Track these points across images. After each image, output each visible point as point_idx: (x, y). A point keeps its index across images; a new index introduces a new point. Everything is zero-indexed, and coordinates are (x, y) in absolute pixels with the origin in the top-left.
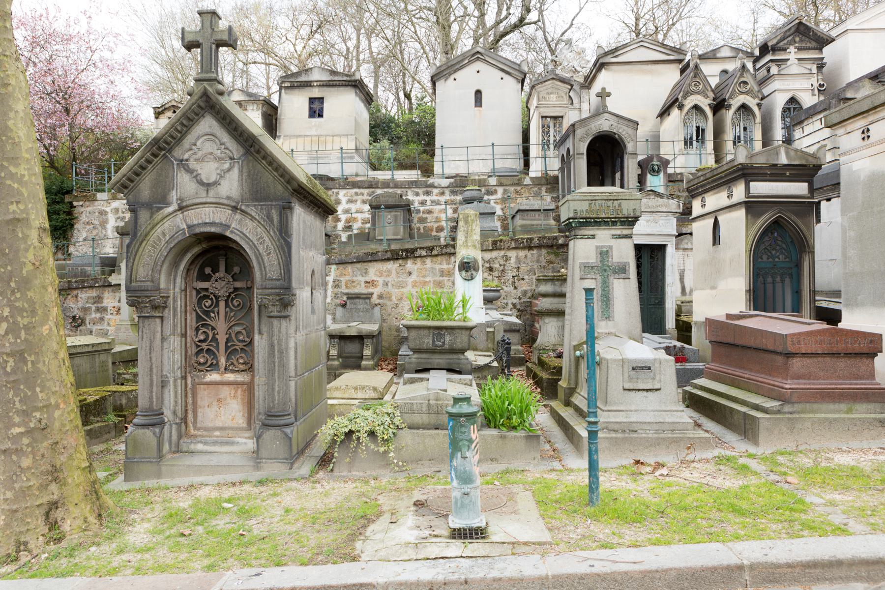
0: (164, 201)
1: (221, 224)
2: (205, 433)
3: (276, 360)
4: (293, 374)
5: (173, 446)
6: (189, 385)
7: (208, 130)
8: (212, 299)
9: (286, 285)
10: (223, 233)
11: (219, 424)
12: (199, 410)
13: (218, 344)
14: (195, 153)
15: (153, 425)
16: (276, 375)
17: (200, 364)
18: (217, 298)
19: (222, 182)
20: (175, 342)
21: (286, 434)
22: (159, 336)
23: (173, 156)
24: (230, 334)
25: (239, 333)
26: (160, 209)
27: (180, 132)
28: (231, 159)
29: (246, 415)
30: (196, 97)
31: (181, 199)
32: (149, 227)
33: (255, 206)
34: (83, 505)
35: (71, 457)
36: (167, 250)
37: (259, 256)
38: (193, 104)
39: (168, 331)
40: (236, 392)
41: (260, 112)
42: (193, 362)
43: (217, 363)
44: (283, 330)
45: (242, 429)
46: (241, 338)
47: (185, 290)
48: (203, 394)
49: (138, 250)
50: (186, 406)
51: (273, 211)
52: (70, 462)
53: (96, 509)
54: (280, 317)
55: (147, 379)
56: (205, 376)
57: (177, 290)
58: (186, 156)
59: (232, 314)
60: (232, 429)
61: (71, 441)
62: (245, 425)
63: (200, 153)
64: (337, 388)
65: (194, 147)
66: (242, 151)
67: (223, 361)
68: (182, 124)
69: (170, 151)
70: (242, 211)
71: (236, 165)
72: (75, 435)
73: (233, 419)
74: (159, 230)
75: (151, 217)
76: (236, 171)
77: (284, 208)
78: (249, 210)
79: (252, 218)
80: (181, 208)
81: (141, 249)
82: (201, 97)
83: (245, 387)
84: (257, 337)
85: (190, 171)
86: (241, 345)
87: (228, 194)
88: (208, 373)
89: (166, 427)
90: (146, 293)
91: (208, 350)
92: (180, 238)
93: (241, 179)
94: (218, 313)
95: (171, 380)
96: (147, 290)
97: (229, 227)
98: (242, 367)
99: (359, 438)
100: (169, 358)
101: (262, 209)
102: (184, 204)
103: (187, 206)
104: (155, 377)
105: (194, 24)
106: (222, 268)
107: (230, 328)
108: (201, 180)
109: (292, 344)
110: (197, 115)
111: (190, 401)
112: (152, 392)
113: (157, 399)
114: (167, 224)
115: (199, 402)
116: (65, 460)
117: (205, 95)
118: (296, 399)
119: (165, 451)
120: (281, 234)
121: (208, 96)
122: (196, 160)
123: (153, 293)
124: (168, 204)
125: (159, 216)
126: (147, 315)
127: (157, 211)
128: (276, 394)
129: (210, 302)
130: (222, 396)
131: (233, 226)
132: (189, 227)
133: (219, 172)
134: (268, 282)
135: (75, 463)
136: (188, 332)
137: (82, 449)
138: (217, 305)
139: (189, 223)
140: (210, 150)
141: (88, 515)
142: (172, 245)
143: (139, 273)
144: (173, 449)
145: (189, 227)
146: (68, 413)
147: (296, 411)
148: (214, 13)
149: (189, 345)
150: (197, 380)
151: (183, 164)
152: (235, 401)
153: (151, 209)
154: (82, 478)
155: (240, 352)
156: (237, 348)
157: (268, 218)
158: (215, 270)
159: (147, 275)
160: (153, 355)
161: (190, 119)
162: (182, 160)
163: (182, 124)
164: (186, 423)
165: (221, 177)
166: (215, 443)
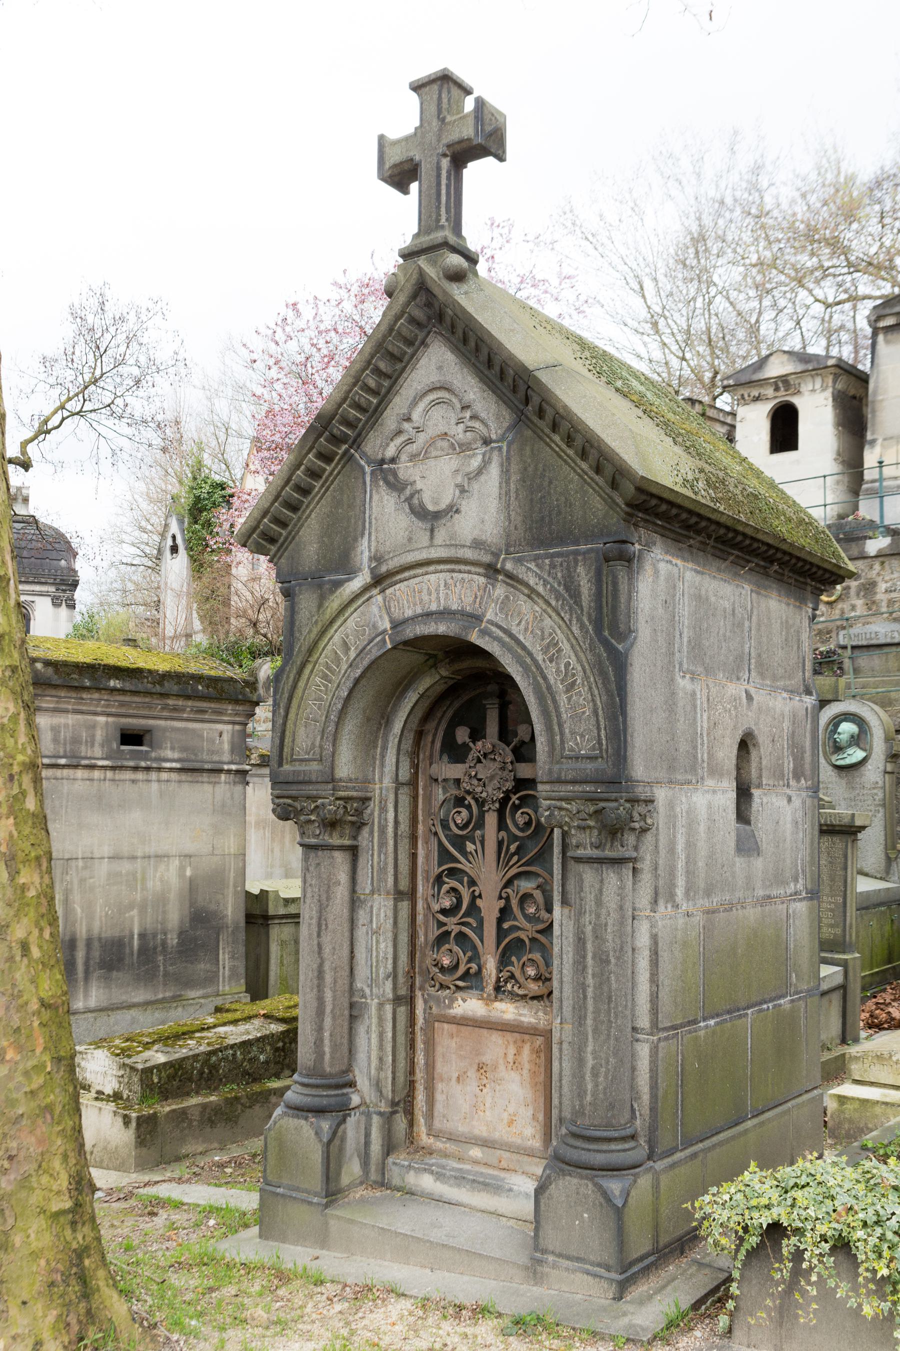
0: (344, 565)
1: (463, 613)
2: (450, 1147)
3: (590, 981)
4: (644, 1022)
5: (373, 1168)
6: (420, 1021)
7: (434, 378)
8: (469, 808)
9: (610, 771)
10: (463, 636)
11: (481, 1130)
12: (439, 1086)
13: (481, 922)
14: (410, 441)
15: (319, 1111)
17: (442, 969)
18: (481, 803)
19: (464, 506)
20: (380, 910)
21: (606, 1196)
22: (341, 893)
23: (364, 455)
24: (508, 899)
25: (525, 898)
26: (338, 584)
27: (374, 392)
28: (486, 442)
29: (541, 1117)
30: (402, 298)
31: (378, 558)
32: (315, 631)
33: (536, 559)
34: (38, 1308)
35: (24, 1183)
36: (350, 684)
37: (545, 694)
38: (397, 318)
40: (518, 1053)
41: (828, 393)
42: (429, 961)
43: (479, 971)
44: (610, 899)
45: (530, 1153)
46: (532, 910)
47: (413, 783)
48: (448, 1043)
50: (412, 1072)
51: (580, 569)
52: (23, 1194)
53: (72, 1319)
54: (600, 861)
56: (452, 1000)
58: (390, 452)
59: (513, 848)
61: (30, 1142)
63: (422, 438)
64: (880, 1057)
65: (406, 426)
66: (507, 417)
68: (377, 371)
69: (357, 442)
70: (510, 576)
71: (495, 454)
72: (43, 1128)
73: (511, 1123)
74: (336, 638)
75: (320, 606)
76: (494, 471)
77: (607, 560)
78: (520, 572)
79: (532, 594)
80: (380, 581)
81: (301, 684)
82: (414, 296)
85: (396, 485)
87: (476, 533)
88: (459, 995)
89: (351, 1121)
90: (311, 790)
92: (376, 653)
93: (505, 495)
95: (374, 1004)
96: (310, 782)
99: (798, 1255)
101: (553, 566)
102: (384, 569)
104: (328, 995)
105: (403, 117)
106: (492, 728)
107: (509, 883)
108: (422, 505)
109: (643, 940)
110: (410, 343)
111: (420, 1059)
113: (335, 1047)
114: (352, 621)
115: (440, 1067)
116: (9, 1188)
117: (422, 289)
118: (654, 1097)
119: (345, 1180)
120: (598, 629)
121: (428, 291)
122: (413, 457)
124: (352, 572)
125: (334, 603)
127: (332, 592)
128: (588, 1077)
129: (465, 813)
130: (487, 1058)
131: (489, 616)
133: (459, 479)
134: (567, 765)
135: (35, 1198)
136: (420, 888)
137: (57, 1164)
138: (480, 824)
139: (397, 614)
140: (442, 429)
141: (46, 1335)
143: (298, 741)
146: (26, 1074)
147: (653, 1129)
148: (445, 79)
149: (420, 918)
151: (385, 471)
152: (514, 1076)
153: (320, 586)
154: (47, 1239)
155: (524, 949)
156: (522, 935)
157: (567, 588)
158: (477, 734)
160: (326, 939)
161: (394, 358)
162: (382, 462)
163: (377, 371)
164: (410, 1113)
165: (463, 491)
166: (460, 1179)
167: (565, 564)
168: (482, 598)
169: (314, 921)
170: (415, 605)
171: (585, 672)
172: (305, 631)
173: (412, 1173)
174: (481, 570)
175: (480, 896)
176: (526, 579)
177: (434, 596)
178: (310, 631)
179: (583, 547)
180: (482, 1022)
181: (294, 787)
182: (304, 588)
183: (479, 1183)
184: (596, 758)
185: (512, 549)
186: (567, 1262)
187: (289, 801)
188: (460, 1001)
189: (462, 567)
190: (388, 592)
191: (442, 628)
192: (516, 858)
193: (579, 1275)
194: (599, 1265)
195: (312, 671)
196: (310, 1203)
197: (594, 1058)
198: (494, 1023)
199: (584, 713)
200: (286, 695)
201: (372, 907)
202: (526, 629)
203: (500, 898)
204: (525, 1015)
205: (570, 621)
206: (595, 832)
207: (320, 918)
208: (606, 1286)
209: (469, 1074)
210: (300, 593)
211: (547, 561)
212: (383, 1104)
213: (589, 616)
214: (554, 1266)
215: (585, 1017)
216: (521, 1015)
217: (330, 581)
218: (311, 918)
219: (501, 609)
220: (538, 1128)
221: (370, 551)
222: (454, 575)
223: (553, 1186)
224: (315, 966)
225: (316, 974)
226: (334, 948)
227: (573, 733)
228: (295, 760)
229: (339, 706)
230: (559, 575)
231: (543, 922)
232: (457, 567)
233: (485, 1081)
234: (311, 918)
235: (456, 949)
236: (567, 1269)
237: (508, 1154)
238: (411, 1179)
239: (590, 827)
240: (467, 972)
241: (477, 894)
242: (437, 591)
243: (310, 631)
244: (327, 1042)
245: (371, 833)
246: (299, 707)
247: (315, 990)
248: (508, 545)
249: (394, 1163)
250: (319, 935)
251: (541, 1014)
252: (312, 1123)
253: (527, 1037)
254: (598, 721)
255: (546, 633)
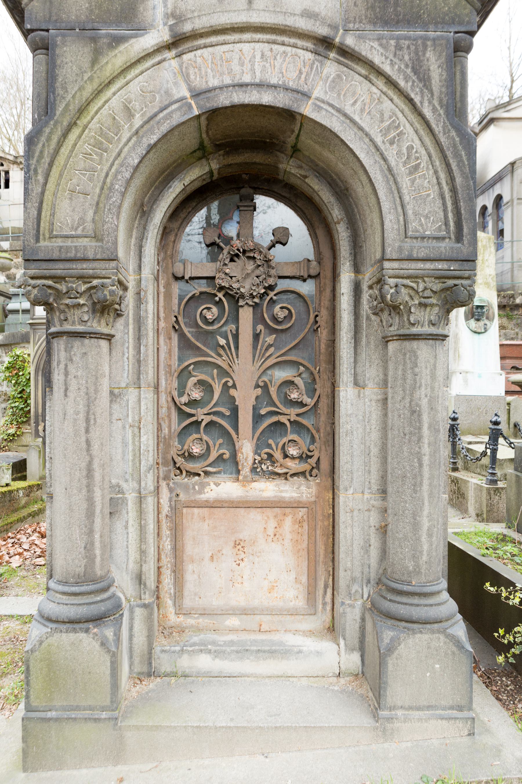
2: (203, 621)
3: (426, 449)
5: (137, 660)
10: (294, 108)
11: (238, 599)
15: (97, 619)
16: (425, 487)
17: (190, 457)
29: (304, 579)
31: (177, 17)
32: (89, 89)
33: (379, 39)
39: (125, 377)
45: (293, 613)
46: (294, 396)
48: (199, 529)
49: (57, 151)
55: (79, 500)
56: (203, 486)
57: (147, 272)
60: (271, 612)
62: (301, 603)
67: (247, 450)
73: (271, 589)
75: (94, 62)
80: (178, 42)
81: (64, 151)
83: (302, 512)
84: (346, 393)
86: (293, 412)
88: (209, 480)
90: (86, 268)
91: (211, 424)
92: (177, 118)
94: (236, 337)
96: (85, 260)
97: (307, 96)
98: (294, 466)
100: (125, 444)
101: (399, 47)
102: (187, 27)
103: (195, 35)
112: (91, 532)
114: (136, 85)
123: (100, 268)
124: (142, 29)
125: (118, 58)
126: (80, 328)
128: (424, 539)
129: (215, 310)
130: (245, 534)
132: (197, 95)
139: (199, 83)
142: (154, 139)
143: (60, 215)
144: (137, 668)
145: (197, 95)
150: (183, 497)
153: (94, 40)
155: (299, 430)
156: (283, 419)
157: (415, 71)
159: (82, 220)
166: (243, 651)
167: (413, 48)
168: (308, 74)
169: (82, 416)
170: (222, 74)
171: (430, 156)
172: (73, 89)
173: (185, 656)
174: (310, 45)
175: (234, 386)
176: (370, 56)
177: (247, 66)
178: (81, 89)
179: (431, 34)
180: (239, 502)
181: (61, 265)
182: (69, 39)
183: (264, 652)
184: (444, 238)
185: (351, 26)
186: (417, 713)
187: (50, 282)
188: (213, 486)
189: (286, 39)
190: (185, 57)
191: (266, 98)
192: (272, 350)
193: (433, 722)
194: (452, 708)
195: (80, 137)
196: (97, 720)
197: (429, 521)
198: (253, 502)
199: (429, 195)
200: (47, 160)
201: (128, 401)
202: (362, 110)
203: (257, 386)
204: (286, 491)
205: (421, 103)
206: (437, 309)
207: (88, 413)
208: (461, 725)
209: (224, 552)
210: (64, 43)
211: (393, 42)
212: (147, 596)
213: (441, 101)
214: (406, 720)
215: (421, 484)
216: (282, 491)
217: (108, 35)
218: (77, 413)
219: (332, 88)
220: (301, 589)
221: (165, 6)
222: (275, 47)
223: (402, 646)
224: (84, 465)
225: (84, 473)
226: (102, 444)
227: (415, 214)
228: (56, 237)
229: (128, 175)
230: (407, 57)
231: (306, 405)
232: (280, 38)
233: (243, 556)
234: (77, 413)
235: (205, 438)
236: (420, 720)
237: (269, 617)
238: (185, 663)
239: (432, 305)
240: (220, 457)
241: (230, 384)
242: (252, 61)
243: (81, 89)
244: (97, 544)
245: (127, 325)
246: (61, 176)
247: (84, 491)
248: (347, 21)
249: (163, 651)
250: (87, 431)
251: (303, 488)
252: (95, 634)
253: (288, 510)
254: (444, 204)
255: (386, 116)
